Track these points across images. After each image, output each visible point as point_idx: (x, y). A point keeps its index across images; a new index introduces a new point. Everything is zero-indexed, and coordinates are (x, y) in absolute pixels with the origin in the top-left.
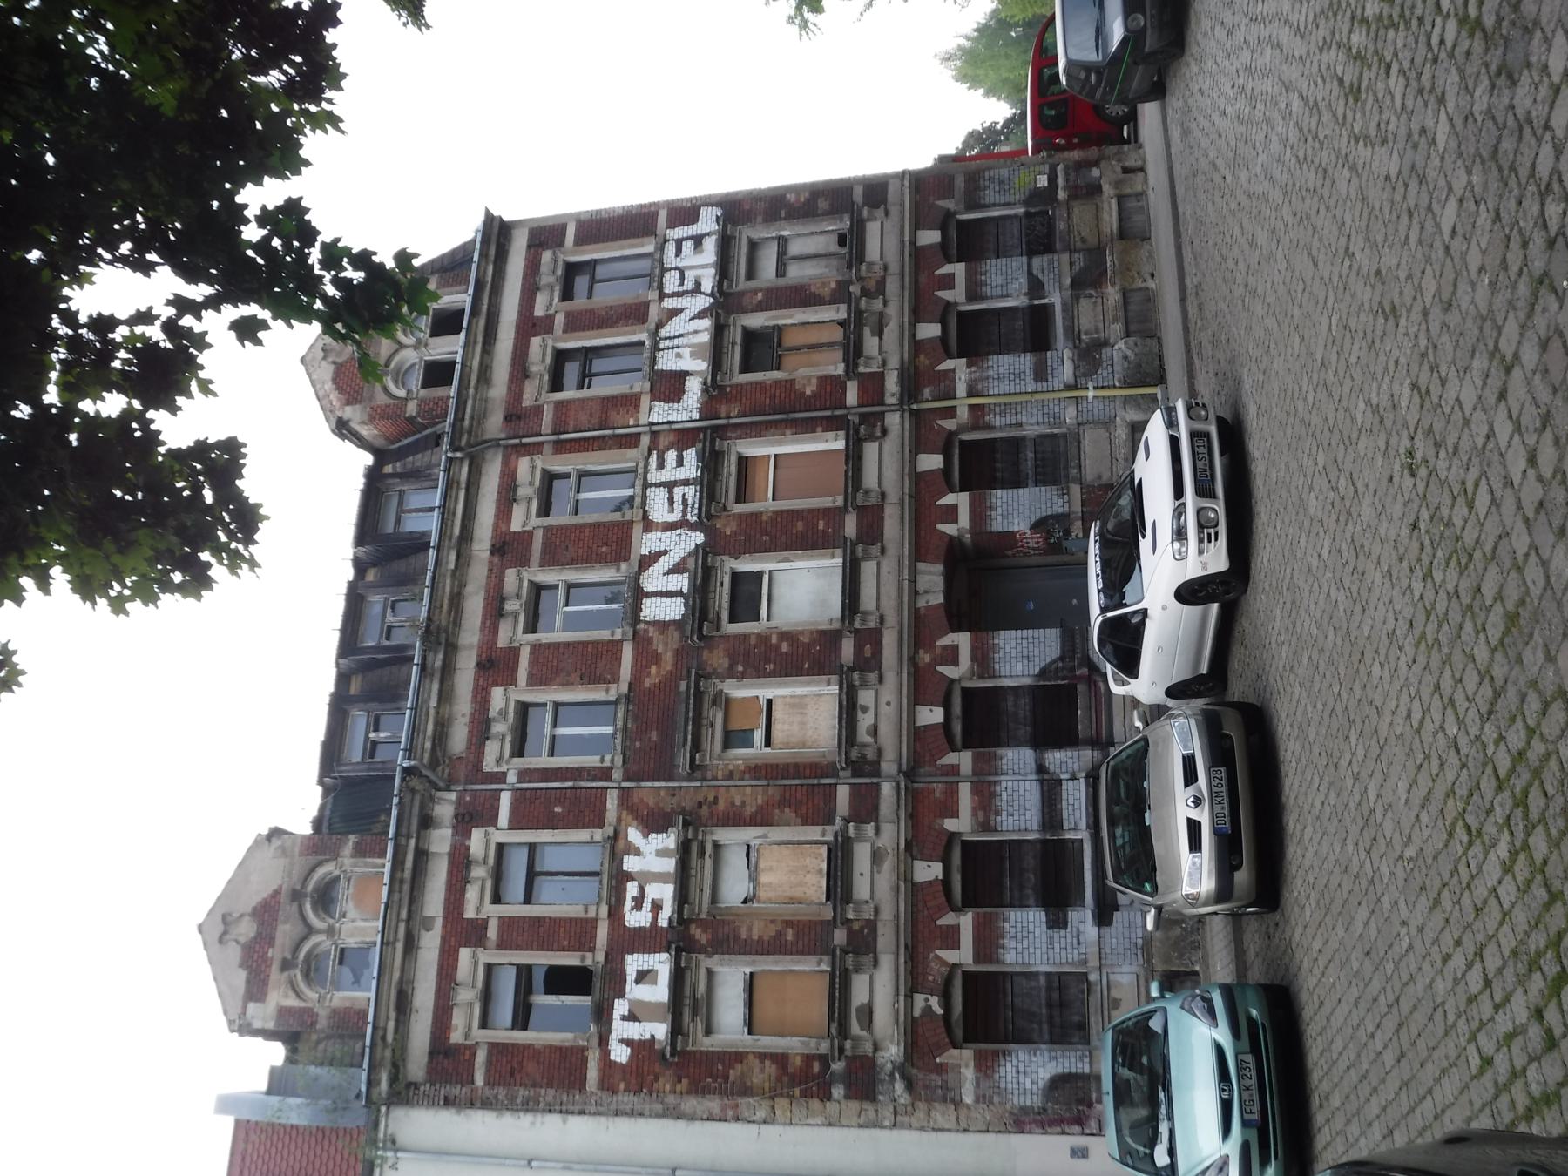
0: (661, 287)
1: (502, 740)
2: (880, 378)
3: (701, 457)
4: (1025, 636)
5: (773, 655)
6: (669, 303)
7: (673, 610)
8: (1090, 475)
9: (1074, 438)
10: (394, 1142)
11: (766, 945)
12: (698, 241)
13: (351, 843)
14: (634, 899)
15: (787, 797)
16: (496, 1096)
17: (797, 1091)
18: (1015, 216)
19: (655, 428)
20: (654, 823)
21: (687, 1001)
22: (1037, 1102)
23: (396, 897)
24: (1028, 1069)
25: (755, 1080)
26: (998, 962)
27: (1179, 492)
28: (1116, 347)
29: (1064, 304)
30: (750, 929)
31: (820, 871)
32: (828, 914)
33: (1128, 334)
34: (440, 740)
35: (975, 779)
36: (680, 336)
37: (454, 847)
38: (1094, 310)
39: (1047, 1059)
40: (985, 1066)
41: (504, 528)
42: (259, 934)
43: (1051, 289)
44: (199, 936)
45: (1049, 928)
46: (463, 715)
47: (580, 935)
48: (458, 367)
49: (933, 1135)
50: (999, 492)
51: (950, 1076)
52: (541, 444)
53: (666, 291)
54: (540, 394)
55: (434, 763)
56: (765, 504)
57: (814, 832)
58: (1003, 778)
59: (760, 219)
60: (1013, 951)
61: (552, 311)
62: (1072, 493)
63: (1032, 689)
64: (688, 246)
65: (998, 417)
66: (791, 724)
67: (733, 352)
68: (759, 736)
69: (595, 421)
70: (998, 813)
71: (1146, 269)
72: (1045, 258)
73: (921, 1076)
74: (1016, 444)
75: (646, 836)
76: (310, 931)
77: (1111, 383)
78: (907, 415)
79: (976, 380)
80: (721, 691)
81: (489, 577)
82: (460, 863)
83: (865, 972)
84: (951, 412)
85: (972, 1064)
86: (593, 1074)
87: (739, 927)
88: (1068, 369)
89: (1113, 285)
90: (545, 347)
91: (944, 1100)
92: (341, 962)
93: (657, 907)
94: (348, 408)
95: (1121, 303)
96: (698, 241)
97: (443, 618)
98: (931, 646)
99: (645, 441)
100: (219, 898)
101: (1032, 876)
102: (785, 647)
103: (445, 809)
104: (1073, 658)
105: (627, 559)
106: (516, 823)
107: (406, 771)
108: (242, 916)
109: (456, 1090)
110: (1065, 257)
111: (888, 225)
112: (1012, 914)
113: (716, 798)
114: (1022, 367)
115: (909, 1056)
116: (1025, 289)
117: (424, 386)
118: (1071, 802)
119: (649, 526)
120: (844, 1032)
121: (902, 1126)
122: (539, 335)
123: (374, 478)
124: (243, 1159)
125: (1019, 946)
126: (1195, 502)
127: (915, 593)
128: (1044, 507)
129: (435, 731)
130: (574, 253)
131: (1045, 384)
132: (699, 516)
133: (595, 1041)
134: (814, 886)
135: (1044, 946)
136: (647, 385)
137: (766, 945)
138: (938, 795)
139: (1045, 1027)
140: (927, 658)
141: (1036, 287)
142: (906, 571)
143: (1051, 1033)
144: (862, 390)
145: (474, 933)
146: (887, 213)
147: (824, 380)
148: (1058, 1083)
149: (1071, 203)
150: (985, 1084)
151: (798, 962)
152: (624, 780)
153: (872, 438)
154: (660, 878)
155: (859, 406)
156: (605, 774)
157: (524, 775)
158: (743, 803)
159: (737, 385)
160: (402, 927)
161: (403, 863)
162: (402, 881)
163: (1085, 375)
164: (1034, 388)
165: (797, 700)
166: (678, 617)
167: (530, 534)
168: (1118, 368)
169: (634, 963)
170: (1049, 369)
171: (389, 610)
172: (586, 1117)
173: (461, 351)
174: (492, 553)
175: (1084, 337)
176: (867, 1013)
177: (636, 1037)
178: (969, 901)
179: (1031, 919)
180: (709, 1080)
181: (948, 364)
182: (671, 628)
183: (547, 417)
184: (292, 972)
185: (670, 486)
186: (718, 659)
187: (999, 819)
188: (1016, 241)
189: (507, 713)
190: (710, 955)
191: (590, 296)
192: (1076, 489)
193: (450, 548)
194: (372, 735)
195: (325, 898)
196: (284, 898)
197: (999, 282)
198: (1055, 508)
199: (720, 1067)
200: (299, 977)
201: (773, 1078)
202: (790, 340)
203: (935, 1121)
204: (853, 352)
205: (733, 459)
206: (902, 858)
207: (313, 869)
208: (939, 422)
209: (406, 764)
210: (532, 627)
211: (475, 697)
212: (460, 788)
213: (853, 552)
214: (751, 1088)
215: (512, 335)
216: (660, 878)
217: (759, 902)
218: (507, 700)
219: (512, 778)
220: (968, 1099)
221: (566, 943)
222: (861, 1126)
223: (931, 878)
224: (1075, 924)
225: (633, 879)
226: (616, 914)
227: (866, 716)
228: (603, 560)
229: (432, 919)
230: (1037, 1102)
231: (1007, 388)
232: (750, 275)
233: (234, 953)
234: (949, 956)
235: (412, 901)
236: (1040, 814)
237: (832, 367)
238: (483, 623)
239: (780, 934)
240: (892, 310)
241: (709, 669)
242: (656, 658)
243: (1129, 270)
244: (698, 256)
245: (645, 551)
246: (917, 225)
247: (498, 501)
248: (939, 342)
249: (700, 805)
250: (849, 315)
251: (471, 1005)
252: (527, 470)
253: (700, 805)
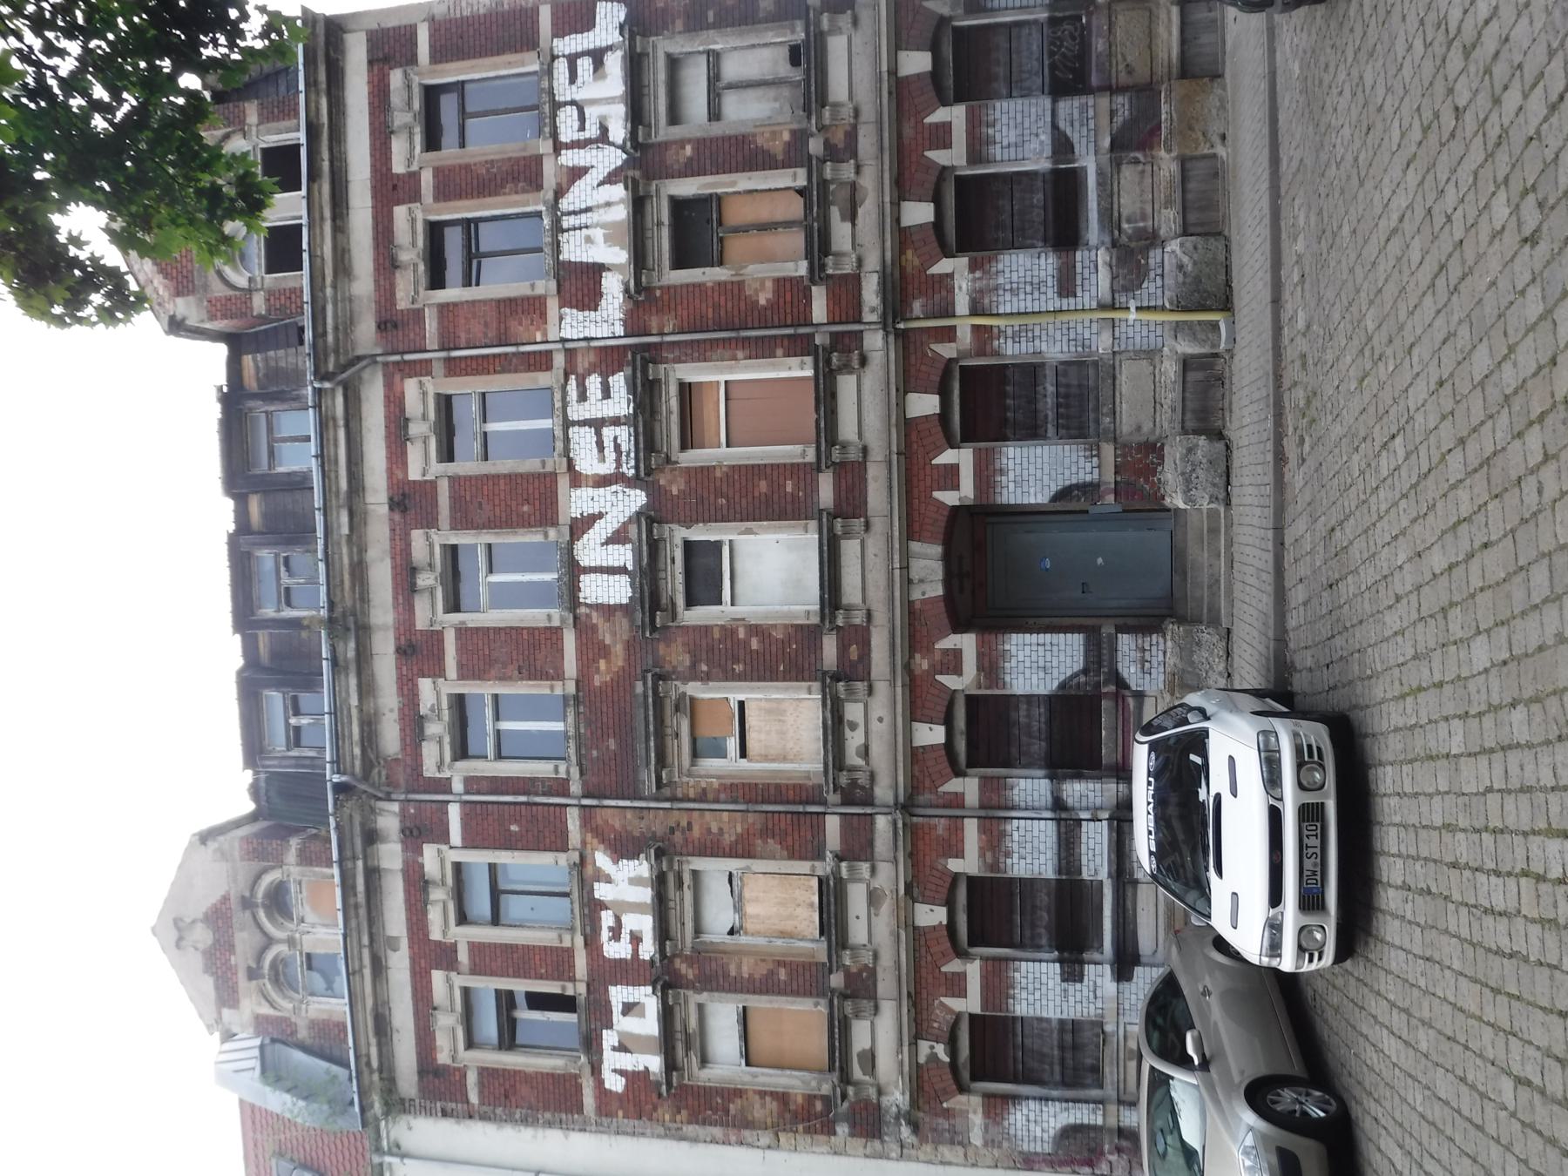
0: (555, 134)
1: (440, 742)
2: (855, 280)
3: (632, 387)
4: (1041, 641)
5: (742, 652)
6: (569, 158)
7: (618, 591)
8: (1126, 426)
9: (1107, 370)
10: (398, 1146)
11: (757, 984)
12: (598, 56)
14: (611, 929)
15: (770, 826)
17: (801, 1127)
18: (1036, 22)
19: (569, 345)
20: (623, 848)
21: (679, 1036)
22: (1048, 1148)
23: (353, 923)
24: (1039, 1119)
25: (756, 1115)
26: (989, 161)
27: (1276, 897)
28: (1168, 249)
29: (1100, 173)
30: (739, 967)
31: (812, 905)
32: (820, 951)
33: (1185, 232)
34: (370, 741)
35: (982, 813)
36: (588, 210)
37: (406, 862)
38: (1140, 183)
39: (1058, 1110)
40: (997, 1106)
41: (400, 476)
42: (217, 941)
43: (1084, 151)
44: (155, 939)
45: (1063, 980)
46: (391, 711)
47: (559, 962)
48: (305, 232)
49: (940, 1169)
50: (1016, 638)
51: (958, 1122)
52: (429, 361)
53: (564, 138)
54: (416, 292)
55: (368, 765)
56: (715, 454)
57: (804, 866)
58: (1014, 814)
59: (679, 25)
60: (1024, 1003)
61: (414, 168)
62: (1103, 454)
63: (1050, 700)
64: (585, 65)
65: (1010, 342)
66: (768, 733)
67: (660, 238)
68: (732, 744)
69: (492, 334)
70: (1008, 854)
71: (1215, 128)
72: (1077, 102)
73: (927, 1119)
74: (1032, 371)
75: (616, 862)
76: (269, 941)
77: (1160, 303)
78: (891, 338)
79: (981, 291)
80: (684, 694)
81: (392, 540)
82: (417, 885)
83: (864, 1018)
84: (949, 334)
85: (980, 1110)
86: (589, 1101)
87: (728, 964)
88: (1103, 280)
89: (1169, 151)
90: (413, 221)
91: (952, 1142)
92: (310, 968)
93: (636, 939)
94: (180, 301)
95: (1178, 179)
96: (598, 56)
97: (347, 598)
98: (929, 650)
99: (559, 360)
100: (166, 901)
101: (1045, 915)
102: (755, 644)
103: (389, 820)
104: (1098, 673)
105: (554, 523)
106: (470, 843)
107: (340, 788)
108: (194, 922)
109: (450, 1106)
110: (1104, 102)
111: (858, 40)
112: (998, 105)
113: (689, 824)
114: (1043, 274)
115: (914, 1103)
116: (1048, 151)
117: (270, 270)
118: (1091, 846)
119: (577, 480)
120: (846, 1078)
121: (909, 1159)
122: (404, 202)
123: (234, 401)
124: (253, 1123)
125: (1031, 998)
126: (1296, 920)
127: (908, 582)
128: (1067, 472)
129: (362, 731)
130: (432, 73)
131: (1072, 300)
132: (637, 467)
133: (587, 1070)
134: (808, 920)
135: (1058, 998)
136: (553, 285)
137: (757, 984)
138: (940, 831)
139: (1057, 1068)
140: (925, 665)
141: (1062, 146)
142: (897, 557)
143: (1063, 1074)
144: (833, 300)
145: (445, 956)
146: (855, 22)
147: (780, 283)
148: (1070, 1133)
149: (1114, 6)
150: (993, 1130)
151: (793, 1003)
152: (585, 796)
153: (846, 368)
154: (636, 908)
155: (828, 324)
156: (561, 787)
157: (472, 784)
158: (721, 829)
159: (669, 287)
160: (366, 953)
161: (354, 887)
162: (356, 906)
163: (1126, 289)
164: (1058, 305)
165: (774, 705)
166: (625, 601)
167: (433, 485)
168: (1169, 281)
169: (618, 995)
170: (1079, 278)
171: (283, 569)
172: (587, 1134)
173: (304, 213)
174: (391, 509)
175: (1125, 226)
176: (869, 1059)
177: (630, 1068)
178: (969, 436)
179: (1044, 970)
181: (944, 266)
182: (619, 614)
183: (431, 325)
184: (261, 981)
185: (597, 424)
186: (677, 656)
187: (1009, 861)
188: (1036, 64)
189: (440, 710)
190: (700, 991)
191: (462, 145)
192: (1108, 450)
193: (339, 507)
194: (293, 721)
195: (278, 901)
196: (234, 903)
197: (1013, 140)
198: (1081, 475)
200: (269, 986)
201: (775, 1114)
202: (737, 214)
203: (942, 1155)
204: (819, 246)
205: (673, 390)
206: (902, 904)
207: (258, 877)
208: (933, 346)
209: (336, 778)
210: (454, 606)
211: (400, 689)
212: (402, 797)
213: (831, 529)
214: (753, 1122)
215: (369, 202)
216: (636, 908)
217: (746, 933)
218: (438, 694)
219: (458, 786)
221: (543, 971)
222: (866, 1156)
223: (936, 923)
224: (1092, 977)
225: (607, 908)
226: (592, 943)
227: (855, 734)
228: (525, 523)
229: (397, 939)
230: (1048, 1148)
231: (1022, 304)
232: (674, 118)
233: (197, 960)
234: (956, 1004)
235: (371, 922)
236: (1056, 858)
237: (791, 265)
238: (395, 598)
239: (772, 973)
240: (868, 181)
241: (668, 668)
242: (604, 651)
243: (1191, 128)
244: (600, 83)
245: (575, 512)
246: (899, 42)
247: (388, 437)
248: (929, 80)
249: (672, 830)
250: (807, 34)
252: (417, 396)
253: (672, 830)
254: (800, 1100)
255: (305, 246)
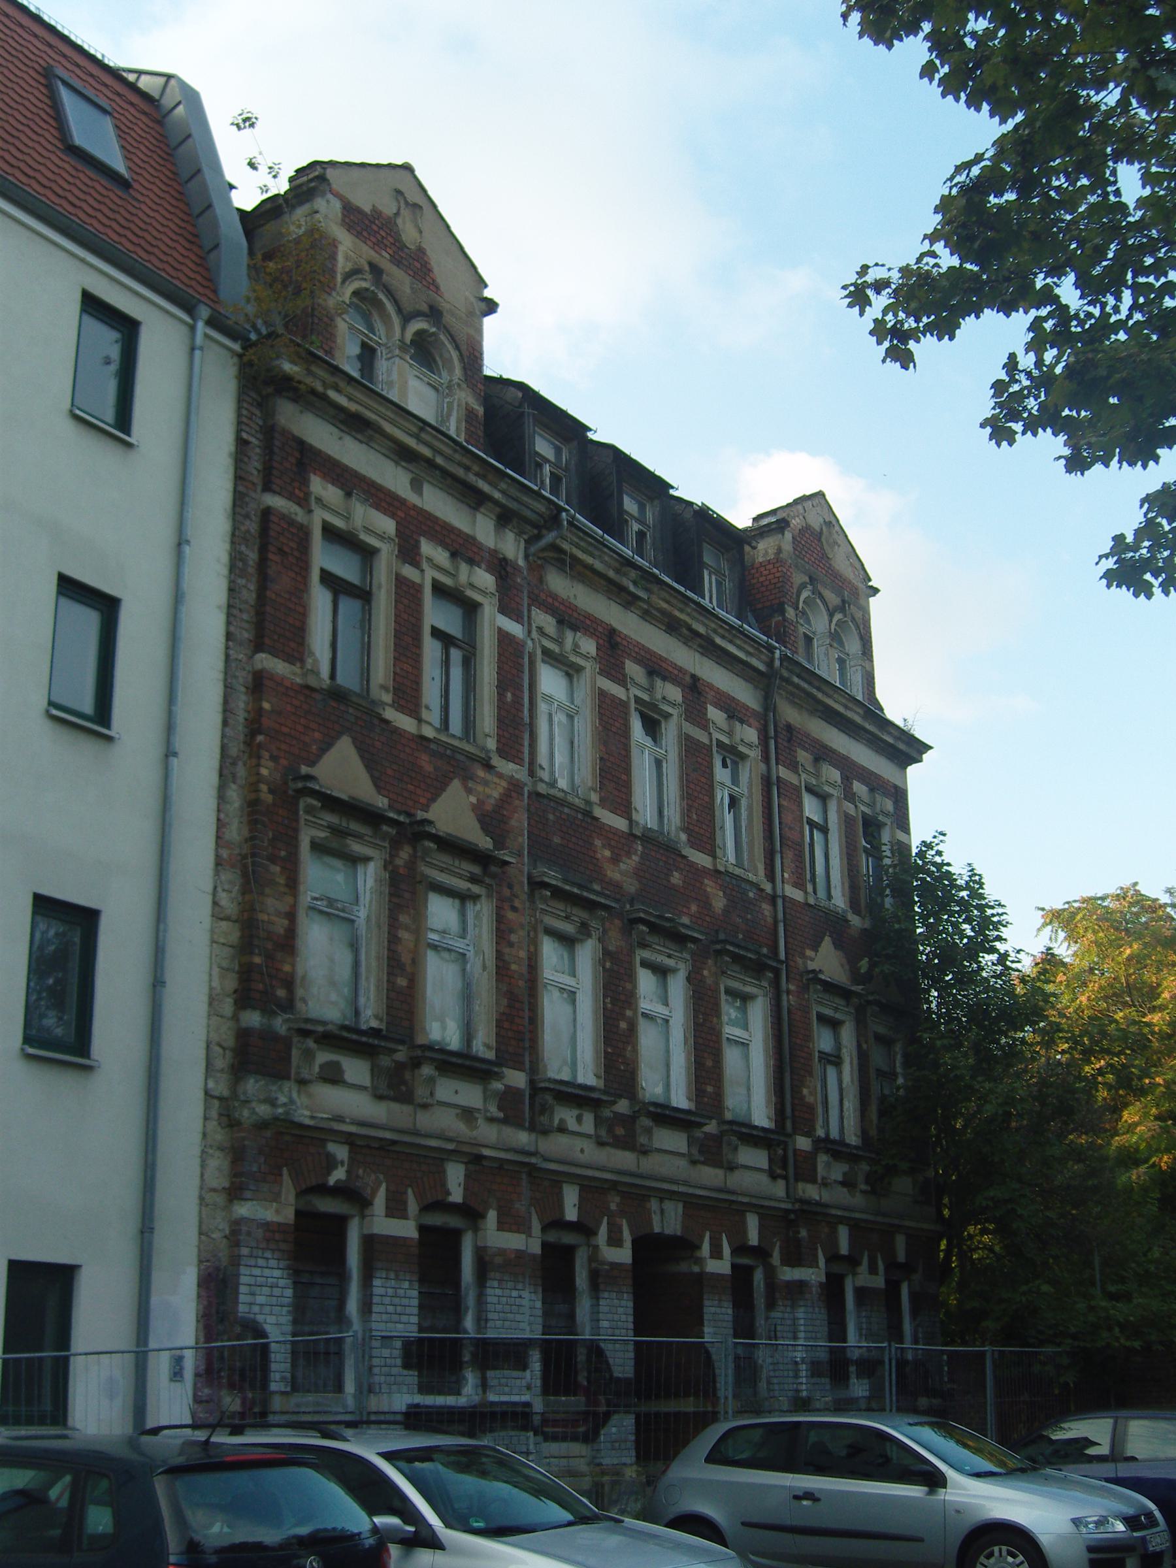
13: (476, 407)
16: (247, 516)
80: (589, 936)
81: (675, 666)
121: (207, 1108)
172: (223, 640)
176: (333, 1076)
180: (271, 834)
199: (283, 853)
220: (243, 1210)
249: (510, 886)
251: (347, 519)
254: (287, 968)
255: (508, 471)
